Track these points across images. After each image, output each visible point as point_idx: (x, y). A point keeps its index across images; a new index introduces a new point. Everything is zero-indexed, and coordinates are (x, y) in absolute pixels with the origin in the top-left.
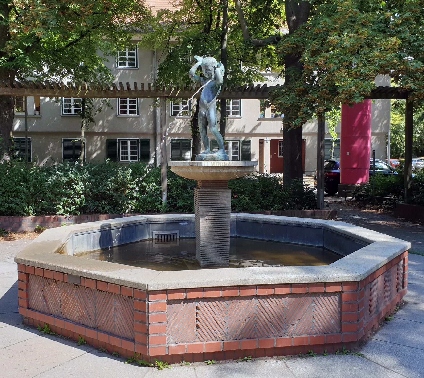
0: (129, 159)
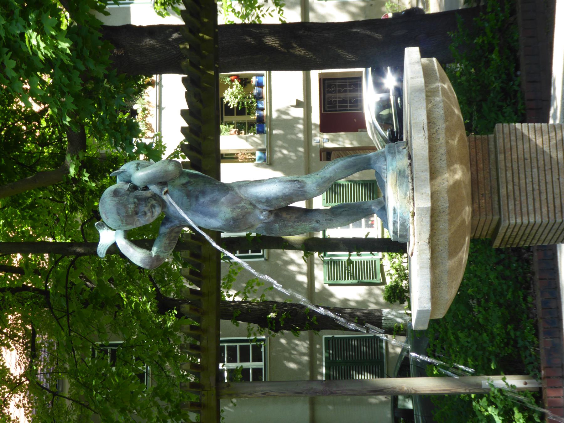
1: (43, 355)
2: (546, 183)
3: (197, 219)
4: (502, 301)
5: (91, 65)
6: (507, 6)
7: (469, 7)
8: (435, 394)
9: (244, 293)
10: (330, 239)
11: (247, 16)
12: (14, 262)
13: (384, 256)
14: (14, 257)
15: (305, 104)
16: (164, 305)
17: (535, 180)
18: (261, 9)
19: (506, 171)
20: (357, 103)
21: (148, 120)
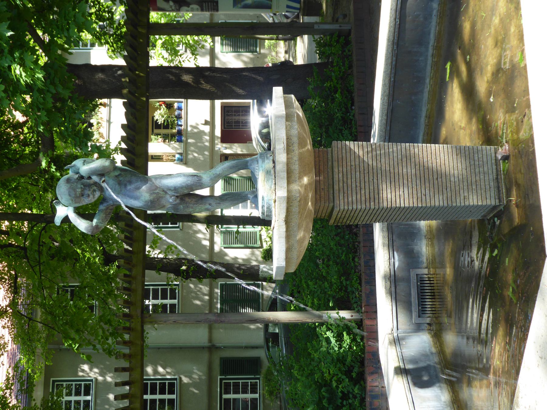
0: (257, 396)
1: (23, 292)
2: (365, 182)
3: (125, 200)
4: (338, 261)
5: (60, 89)
6: (347, 62)
7: (322, 61)
8: (292, 323)
9: (165, 253)
10: (225, 216)
11: (172, 61)
12: (3, 226)
13: (262, 229)
14: (3, 223)
15: (211, 123)
16: (108, 259)
17: (358, 180)
18: (182, 56)
19: (339, 173)
20: (246, 124)
21: (101, 130)
